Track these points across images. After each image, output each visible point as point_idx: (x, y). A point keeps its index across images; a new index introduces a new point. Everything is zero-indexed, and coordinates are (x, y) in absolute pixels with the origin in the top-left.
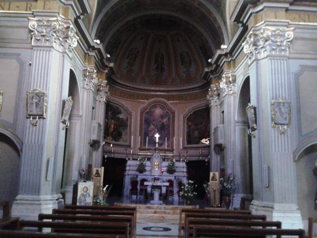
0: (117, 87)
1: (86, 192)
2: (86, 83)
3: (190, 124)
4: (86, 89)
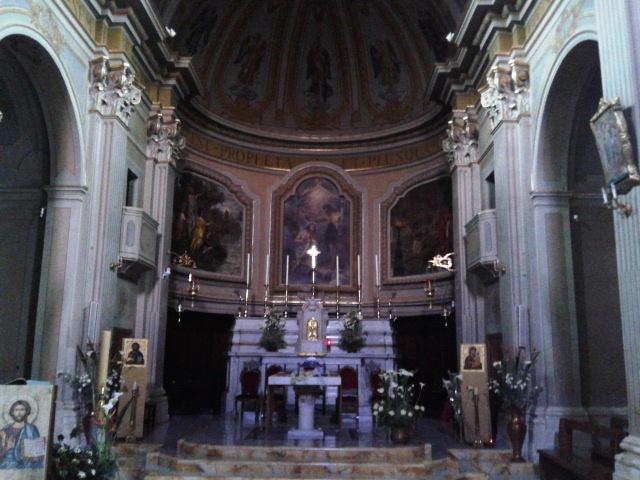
0: (209, 132)
1: (24, 419)
2: (101, 96)
3: (399, 224)
4: (103, 117)
